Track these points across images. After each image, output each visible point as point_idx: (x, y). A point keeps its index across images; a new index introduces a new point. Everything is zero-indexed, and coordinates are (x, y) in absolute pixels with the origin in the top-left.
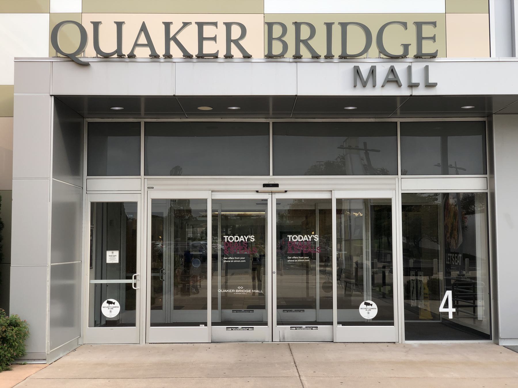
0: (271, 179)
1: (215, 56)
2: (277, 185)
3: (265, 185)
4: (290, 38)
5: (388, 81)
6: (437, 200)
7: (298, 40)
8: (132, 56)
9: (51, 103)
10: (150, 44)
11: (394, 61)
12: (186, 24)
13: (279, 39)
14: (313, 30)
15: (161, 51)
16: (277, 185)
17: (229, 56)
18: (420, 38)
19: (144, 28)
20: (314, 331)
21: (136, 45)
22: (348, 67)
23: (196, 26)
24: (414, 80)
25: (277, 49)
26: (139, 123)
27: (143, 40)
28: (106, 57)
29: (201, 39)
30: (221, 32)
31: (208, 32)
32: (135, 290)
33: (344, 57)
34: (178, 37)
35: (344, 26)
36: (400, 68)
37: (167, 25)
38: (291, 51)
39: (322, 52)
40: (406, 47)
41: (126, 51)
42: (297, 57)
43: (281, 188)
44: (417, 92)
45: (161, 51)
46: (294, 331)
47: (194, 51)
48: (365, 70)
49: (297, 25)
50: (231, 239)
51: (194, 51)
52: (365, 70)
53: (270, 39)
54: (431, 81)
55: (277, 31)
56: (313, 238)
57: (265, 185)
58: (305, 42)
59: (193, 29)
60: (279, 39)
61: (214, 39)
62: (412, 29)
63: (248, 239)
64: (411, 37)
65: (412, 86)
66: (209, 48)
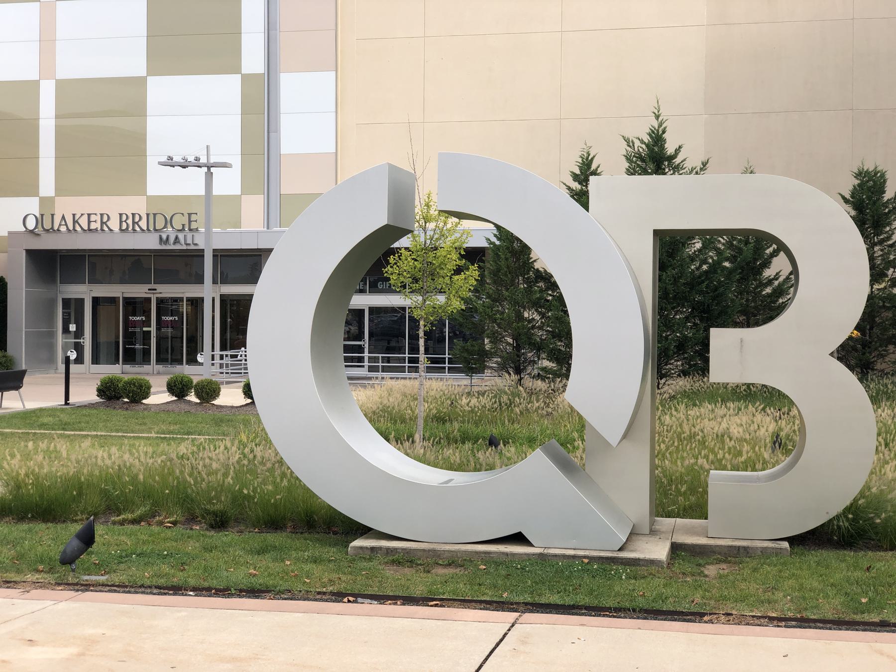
0: (152, 286)
1: (96, 229)
2: (155, 290)
3: (149, 290)
4: (130, 221)
5: (175, 243)
6: (225, 300)
7: (134, 223)
8: (58, 230)
9: (24, 253)
10: (66, 225)
11: (106, 252)
12: (82, 215)
13: (125, 221)
14: (141, 218)
15: (71, 228)
16: (155, 290)
17: (102, 230)
18: (190, 221)
19: (63, 218)
20: (175, 369)
21: (60, 225)
22: (157, 235)
23: (87, 215)
24: (188, 242)
25: (124, 226)
26: (86, 255)
27: (63, 223)
28: (48, 231)
29: (89, 222)
30: (98, 218)
31: (93, 218)
32: (84, 345)
33: (155, 230)
34: (79, 221)
35: (155, 215)
36: (181, 236)
37: (74, 215)
38: (131, 228)
39: (145, 228)
40: (183, 225)
41: (56, 228)
42: (134, 230)
43: (158, 291)
44: (189, 248)
45: (71, 228)
46: (164, 368)
47: (86, 228)
48: (164, 237)
49: (133, 215)
50: (133, 318)
51: (86, 228)
52: (164, 237)
53: (121, 222)
54: (195, 242)
55: (124, 218)
56: (175, 319)
57: (149, 290)
58: (137, 223)
59: (86, 217)
60: (125, 221)
61: (95, 221)
62: (187, 216)
63: (175, 319)
64: (185, 220)
65: (187, 244)
66: (93, 226)
